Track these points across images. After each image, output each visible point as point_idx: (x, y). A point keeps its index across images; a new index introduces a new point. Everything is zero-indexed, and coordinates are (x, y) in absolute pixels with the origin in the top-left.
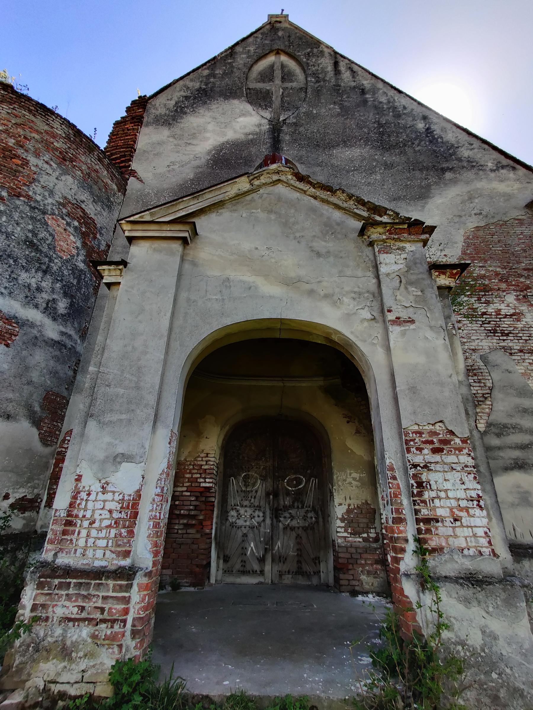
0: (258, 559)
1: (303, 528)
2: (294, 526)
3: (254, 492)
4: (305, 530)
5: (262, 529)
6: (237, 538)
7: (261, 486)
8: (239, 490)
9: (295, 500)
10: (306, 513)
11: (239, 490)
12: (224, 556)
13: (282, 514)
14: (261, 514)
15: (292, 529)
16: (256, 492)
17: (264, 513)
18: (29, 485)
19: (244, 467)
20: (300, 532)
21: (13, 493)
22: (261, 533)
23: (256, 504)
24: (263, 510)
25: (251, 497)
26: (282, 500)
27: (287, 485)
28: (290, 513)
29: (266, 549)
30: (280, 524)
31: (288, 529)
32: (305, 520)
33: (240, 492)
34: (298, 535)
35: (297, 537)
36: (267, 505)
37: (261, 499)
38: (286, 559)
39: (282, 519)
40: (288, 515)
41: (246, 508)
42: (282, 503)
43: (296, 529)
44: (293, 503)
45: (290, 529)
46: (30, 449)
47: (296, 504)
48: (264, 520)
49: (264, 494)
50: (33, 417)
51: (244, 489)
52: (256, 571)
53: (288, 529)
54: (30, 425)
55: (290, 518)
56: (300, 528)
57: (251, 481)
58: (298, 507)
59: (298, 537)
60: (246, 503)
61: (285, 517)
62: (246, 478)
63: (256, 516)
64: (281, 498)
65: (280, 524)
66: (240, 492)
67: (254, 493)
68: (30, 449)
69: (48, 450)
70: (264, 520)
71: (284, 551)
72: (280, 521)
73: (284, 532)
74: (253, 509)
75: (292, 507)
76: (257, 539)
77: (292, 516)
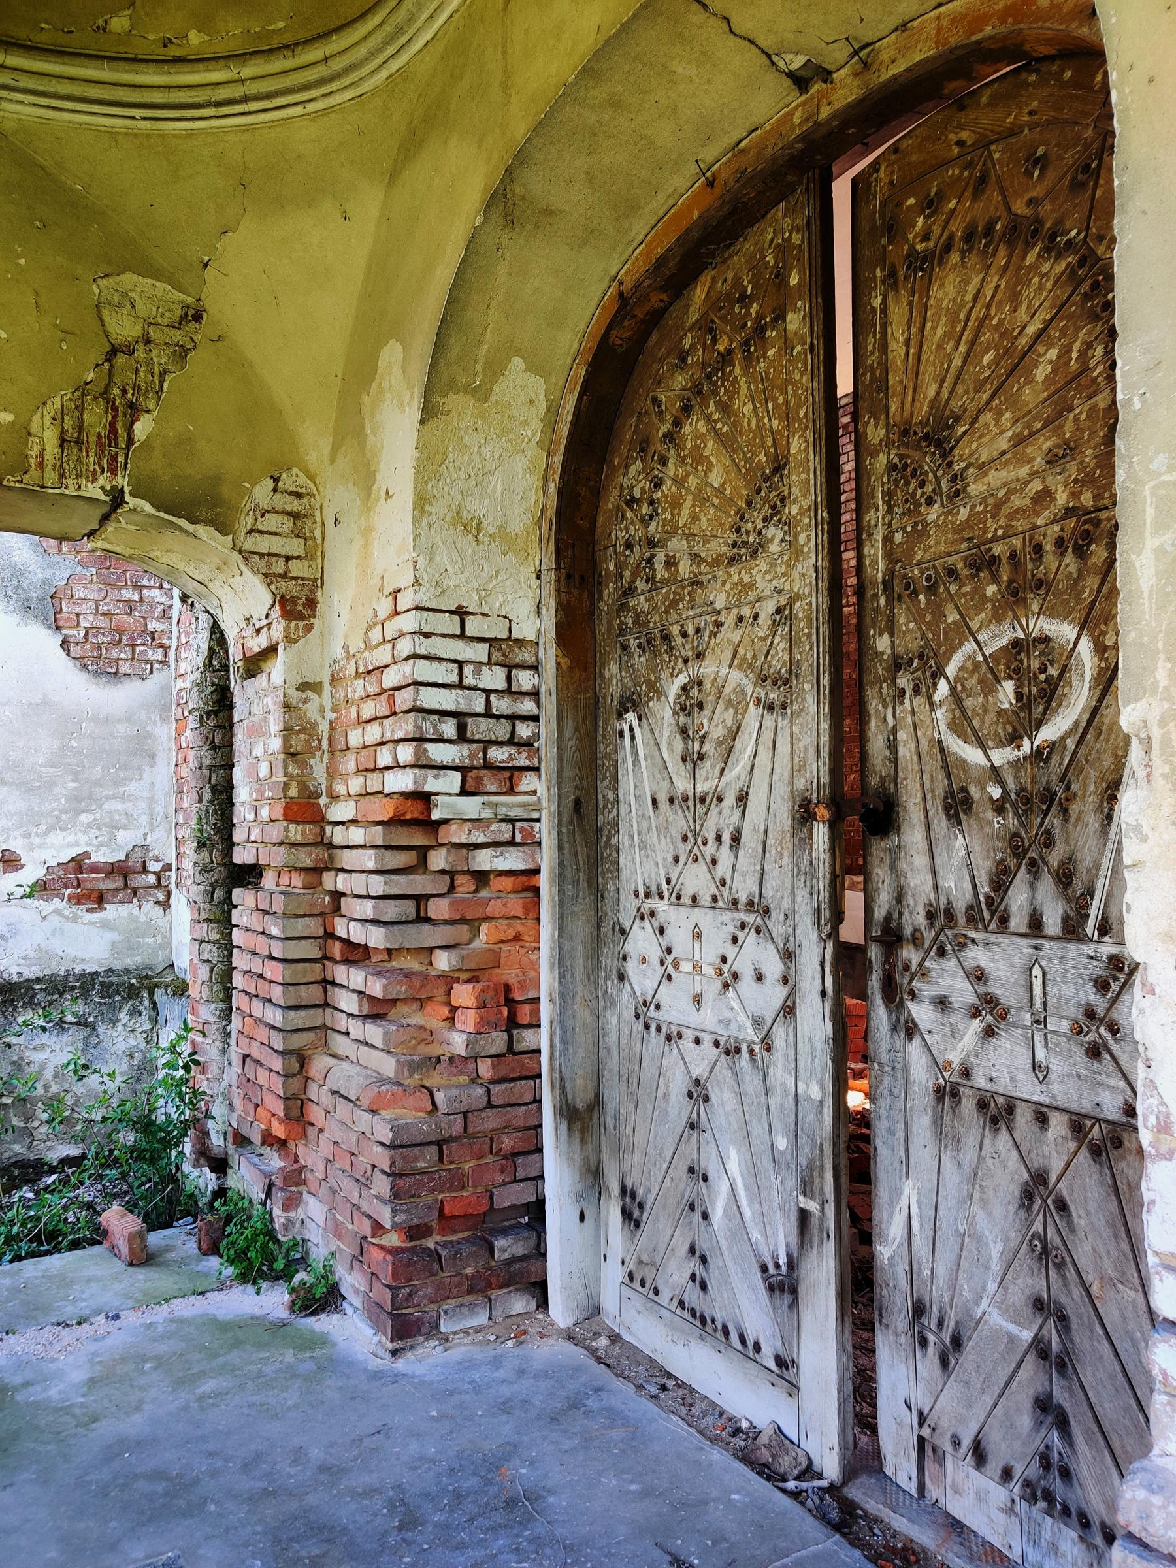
0: (764, 1268)
1: (1078, 1125)
2: (1003, 1085)
3: (730, 800)
4: (1096, 1152)
5: (779, 1073)
6: (666, 1097)
7: (764, 758)
8: (662, 798)
9: (1021, 855)
10: (1102, 986)
11: (662, 798)
12: (624, 1190)
13: (925, 975)
14: (774, 967)
15: (998, 1113)
16: (742, 798)
17: (788, 956)
18: (84, 818)
19: (675, 630)
20: (1054, 1147)
21: (32, 847)
22: (776, 1099)
23: (745, 888)
24: (778, 930)
25: (719, 838)
26: (920, 860)
27: (954, 726)
28: (978, 976)
29: (804, 1216)
30: (915, 1053)
31: (968, 1105)
32: (1094, 1052)
33: (664, 804)
34: (1039, 1178)
35: (1027, 1196)
36: (802, 894)
37: (771, 853)
38: (957, 1342)
39: (922, 1013)
40: (963, 993)
41: (697, 915)
42: (919, 882)
43: (1023, 1117)
44: (1001, 881)
45: (982, 1105)
46: (46, 702)
47: (1018, 900)
48: (789, 1010)
49: (783, 815)
50: (16, 589)
51: (682, 785)
52: (757, 1348)
53: (968, 1105)
54: (14, 619)
55: (975, 1013)
56: (1058, 1125)
57: (715, 722)
58: (1036, 924)
59: (1036, 1188)
60: (696, 880)
61: (942, 1003)
62: (691, 703)
63: (747, 975)
64: (913, 836)
65: (915, 1053)
66: (664, 804)
67: (723, 817)
68: (46, 702)
69: (124, 696)
70: (789, 1010)
71: (942, 1271)
72: (912, 1030)
73: (938, 1123)
74: (730, 919)
75: (990, 913)
76: (758, 1131)
77: (990, 1001)
